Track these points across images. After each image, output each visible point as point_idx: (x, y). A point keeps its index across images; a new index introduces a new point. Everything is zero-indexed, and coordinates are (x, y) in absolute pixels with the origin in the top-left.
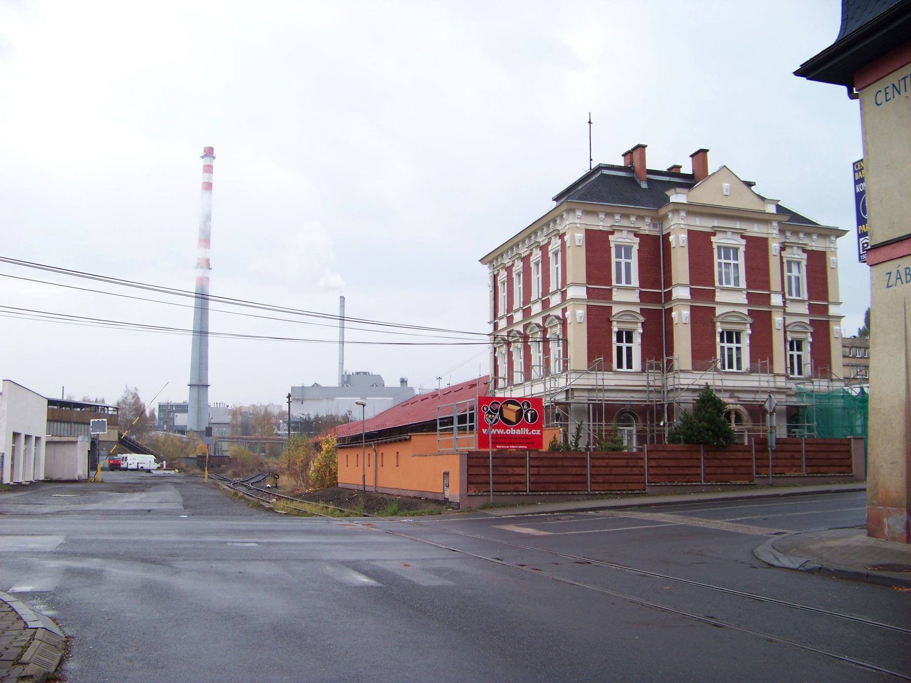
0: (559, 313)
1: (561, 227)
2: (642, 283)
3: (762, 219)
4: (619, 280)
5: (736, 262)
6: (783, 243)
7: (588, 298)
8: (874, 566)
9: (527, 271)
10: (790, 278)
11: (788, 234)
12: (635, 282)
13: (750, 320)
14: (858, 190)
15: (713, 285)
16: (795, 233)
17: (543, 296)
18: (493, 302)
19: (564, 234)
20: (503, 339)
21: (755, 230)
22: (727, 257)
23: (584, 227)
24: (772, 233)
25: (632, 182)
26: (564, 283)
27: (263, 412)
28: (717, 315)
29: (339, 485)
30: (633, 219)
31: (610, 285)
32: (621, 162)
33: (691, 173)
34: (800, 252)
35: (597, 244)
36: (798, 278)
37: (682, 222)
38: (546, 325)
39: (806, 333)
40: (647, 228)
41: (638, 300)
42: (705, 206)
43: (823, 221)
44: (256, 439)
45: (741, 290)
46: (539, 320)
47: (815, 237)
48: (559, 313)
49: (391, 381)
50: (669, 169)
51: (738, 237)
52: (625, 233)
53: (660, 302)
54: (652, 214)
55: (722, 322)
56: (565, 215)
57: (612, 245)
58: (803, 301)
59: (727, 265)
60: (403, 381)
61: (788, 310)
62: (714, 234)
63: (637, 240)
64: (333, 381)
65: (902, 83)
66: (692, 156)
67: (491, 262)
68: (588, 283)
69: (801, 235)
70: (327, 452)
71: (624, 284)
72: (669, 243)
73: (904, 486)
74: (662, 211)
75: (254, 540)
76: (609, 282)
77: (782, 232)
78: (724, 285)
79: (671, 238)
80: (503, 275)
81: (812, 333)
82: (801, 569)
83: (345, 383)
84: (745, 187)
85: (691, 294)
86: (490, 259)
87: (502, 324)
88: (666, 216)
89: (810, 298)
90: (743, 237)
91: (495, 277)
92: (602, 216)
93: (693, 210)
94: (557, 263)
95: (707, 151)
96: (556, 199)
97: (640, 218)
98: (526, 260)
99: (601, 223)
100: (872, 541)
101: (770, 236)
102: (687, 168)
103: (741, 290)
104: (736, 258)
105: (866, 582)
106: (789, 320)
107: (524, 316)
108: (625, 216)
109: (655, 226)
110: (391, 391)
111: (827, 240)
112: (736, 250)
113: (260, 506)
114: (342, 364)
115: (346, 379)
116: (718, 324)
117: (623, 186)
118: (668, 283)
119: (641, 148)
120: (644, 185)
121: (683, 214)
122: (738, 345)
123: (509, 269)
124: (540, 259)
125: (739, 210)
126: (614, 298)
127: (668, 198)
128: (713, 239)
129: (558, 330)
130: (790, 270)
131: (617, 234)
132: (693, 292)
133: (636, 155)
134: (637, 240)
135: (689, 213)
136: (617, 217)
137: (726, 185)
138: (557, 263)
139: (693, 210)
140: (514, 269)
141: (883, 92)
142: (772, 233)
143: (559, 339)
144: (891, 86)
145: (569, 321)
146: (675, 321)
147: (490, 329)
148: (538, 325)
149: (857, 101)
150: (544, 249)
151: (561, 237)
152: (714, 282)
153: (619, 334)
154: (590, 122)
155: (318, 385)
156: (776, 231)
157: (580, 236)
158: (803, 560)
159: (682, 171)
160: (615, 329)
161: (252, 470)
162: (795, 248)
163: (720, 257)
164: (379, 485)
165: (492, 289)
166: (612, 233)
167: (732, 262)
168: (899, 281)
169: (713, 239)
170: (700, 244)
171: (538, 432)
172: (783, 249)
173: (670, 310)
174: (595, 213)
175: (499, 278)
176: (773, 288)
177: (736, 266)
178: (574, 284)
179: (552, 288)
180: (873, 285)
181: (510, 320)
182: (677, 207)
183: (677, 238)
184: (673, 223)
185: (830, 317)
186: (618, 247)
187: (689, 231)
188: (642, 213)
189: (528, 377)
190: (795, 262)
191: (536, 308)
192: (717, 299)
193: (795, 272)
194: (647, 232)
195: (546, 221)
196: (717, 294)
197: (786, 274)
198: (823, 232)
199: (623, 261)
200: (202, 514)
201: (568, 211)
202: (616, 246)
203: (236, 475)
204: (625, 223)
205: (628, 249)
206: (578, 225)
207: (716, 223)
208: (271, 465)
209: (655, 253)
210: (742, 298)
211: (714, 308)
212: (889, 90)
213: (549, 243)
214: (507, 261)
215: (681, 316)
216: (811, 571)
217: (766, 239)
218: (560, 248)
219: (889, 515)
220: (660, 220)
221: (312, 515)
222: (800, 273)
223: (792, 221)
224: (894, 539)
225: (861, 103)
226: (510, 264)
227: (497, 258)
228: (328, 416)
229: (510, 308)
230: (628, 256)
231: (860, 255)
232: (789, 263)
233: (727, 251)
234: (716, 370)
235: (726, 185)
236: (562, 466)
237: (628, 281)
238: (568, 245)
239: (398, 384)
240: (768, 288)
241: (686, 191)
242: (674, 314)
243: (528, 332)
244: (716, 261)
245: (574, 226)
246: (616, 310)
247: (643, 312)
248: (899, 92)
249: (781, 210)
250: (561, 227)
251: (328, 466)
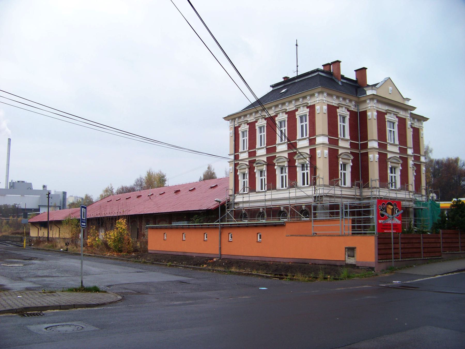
2: (352, 138)
23: (327, 103)
28: (388, 158)
29: (149, 252)
40: (352, 107)
45: (396, 145)
49: (37, 186)
59: (390, 131)
60: (44, 187)
66: (355, 71)
92: (335, 98)
95: (367, 69)
99: (334, 102)
101: (407, 118)
109: (355, 106)
110: (37, 192)
114: (7, 176)
115: (12, 185)
120: (340, 83)
121: (375, 101)
122: (395, 175)
131: (340, 109)
135: (379, 101)
137: (390, 88)
154: (297, 45)
164: (223, 253)
171: (380, 221)
173: (367, 154)
176: (408, 146)
185: (421, 162)
189: (252, 188)
194: (352, 109)
199: (342, 124)
201: (319, 93)
206: (324, 101)
207: (386, 108)
215: (374, 157)
228: (4, 205)
234: (388, 188)
236: (412, 243)
239: (42, 189)
240: (406, 146)
245: (322, 101)
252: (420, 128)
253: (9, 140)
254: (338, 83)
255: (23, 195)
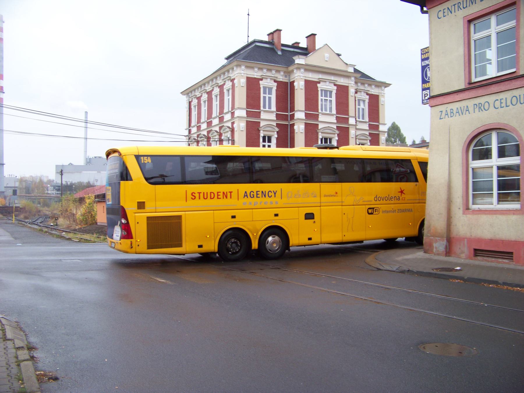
0: (229, 124)
1: (232, 75)
3: (345, 75)
4: (264, 107)
5: (330, 99)
6: (356, 89)
7: (247, 117)
8: (436, 269)
9: (210, 100)
10: (359, 109)
11: (359, 84)
12: (274, 108)
13: (337, 132)
14: (423, 65)
15: (318, 112)
16: (363, 84)
17: (220, 115)
18: (188, 117)
19: (234, 79)
20: (195, 139)
21: (342, 81)
22: (326, 96)
23: (246, 75)
24: (350, 83)
25: (273, 50)
26: (233, 107)
27: (38, 180)
28: (261, 126)
29: (98, 224)
30: (274, 72)
31: (260, 109)
32: (266, 39)
33: (306, 47)
34: (365, 94)
35: (253, 85)
36: (363, 109)
37: (301, 75)
38: (222, 132)
39: (367, 140)
40: (281, 77)
41: (275, 119)
42: (315, 66)
43: (378, 78)
44: (35, 196)
45: (333, 115)
46: (217, 129)
47: (373, 87)
48: (229, 124)
50: (293, 44)
51: (332, 85)
52: (269, 80)
53: (287, 120)
54: (285, 69)
55: (322, 133)
56: (235, 68)
57: (261, 86)
58: (366, 122)
59: (326, 100)
61: (358, 127)
62: (319, 83)
63: (276, 84)
64: (81, 162)
65: (453, 7)
66: (307, 37)
67: (188, 94)
68: (247, 108)
69: (366, 85)
70: (89, 204)
71: (267, 109)
72: (294, 87)
73: (446, 227)
74: (290, 68)
75: (79, 258)
76: (259, 108)
77: (356, 83)
78: (324, 112)
79: (295, 84)
80: (195, 102)
81: (370, 140)
82: (397, 271)
83: (88, 163)
84: (337, 56)
85: (305, 116)
86: (187, 92)
87: (194, 130)
88: (293, 71)
89: (370, 121)
90: (335, 85)
91: (190, 103)
92: (256, 69)
93: (308, 68)
94: (228, 96)
95: (316, 35)
96: (227, 59)
97: (278, 71)
98: (209, 93)
99: (255, 74)
100: (427, 256)
101: (350, 85)
102: (303, 44)
103: (333, 115)
104: (331, 97)
105: (435, 277)
106: (359, 132)
107: (208, 126)
108: (269, 70)
109: (286, 76)
111: (380, 89)
112: (331, 92)
113: (62, 237)
114: (86, 152)
115: (88, 161)
116: (320, 134)
117: (268, 52)
118: (292, 109)
119: (279, 31)
120: (280, 53)
121: (302, 70)
123: (199, 99)
124: (218, 93)
125: (334, 69)
126: (262, 117)
127: (294, 61)
128: (318, 85)
129: (229, 135)
130: (359, 105)
131: (264, 80)
132: (307, 115)
133: (276, 35)
134: (276, 84)
135: (306, 70)
136: (265, 71)
137: (327, 55)
138: (228, 96)
139: (308, 68)
140: (202, 98)
141: (442, 11)
142: (350, 83)
143: (229, 140)
144: (447, 9)
145: (235, 130)
146: (296, 131)
147: (187, 133)
148: (216, 132)
149: (426, 15)
150: (221, 87)
151: (232, 80)
152: (318, 110)
153: (264, 138)
154: (248, 15)
155: (72, 164)
156: (353, 83)
157: (243, 81)
158: (397, 267)
159: (300, 45)
160: (262, 135)
161: (35, 215)
162: (363, 93)
163: (322, 96)
165: (188, 109)
166: (262, 80)
167: (328, 99)
168: (457, 114)
169: (318, 85)
170: (311, 87)
172: (356, 93)
173: (293, 125)
174: (252, 68)
175: (192, 103)
176: (350, 115)
177: (331, 101)
178: (239, 108)
179: (226, 110)
180: (432, 117)
181: (199, 128)
182: (300, 66)
183: (299, 84)
184: (296, 75)
185: (379, 131)
186: (265, 88)
187: (305, 80)
188: (261, 66)
190: (362, 100)
191: (216, 122)
192: (320, 119)
193: (362, 106)
194: (281, 80)
195: (222, 71)
196: (320, 116)
197: (357, 107)
198: (377, 84)
199: (267, 96)
200: (26, 243)
201: (237, 66)
202: (264, 87)
203: (26, 218)
204: (269, 74)
205: (270, 89)
206: (243, 75)
207: (321, 76)
208: (44, 211)
209: (285, 92)
210: (333, 119)
211: (260, 122)
212: (446, 11)
213: (224, 84)
214: (198, 94)
216: (403, 272)
217: (348, 87)
218: (231, 87)
219: (436, 241)
220: (289, 73)
221: (95, 242)
222: (365, 107)
223: (362, 77)
224: (438, 254)
225: (429, 16)
226: (200, 95)
227: (191, 92)
228: (78, 182)
229: (199, 121)
230: (270, 93)
231: (423, 100)
232: (359, 100)
233: (326, 92)
235: (327, 55)
237: (270, 107)
238: (236, 85)
240: (348, 115)
241: (304, 57)
242: (295, 127)
243: (210, 135)
244: (320, 98)
246: (262, 124)
247: (278, 125)
248: (451, 12)
249: (356, 71)
250: (232, 75)
251: (90, 212)
252: (380, 94)
253: (86, 113)
254: (277, 53)
255: (99, 172)
